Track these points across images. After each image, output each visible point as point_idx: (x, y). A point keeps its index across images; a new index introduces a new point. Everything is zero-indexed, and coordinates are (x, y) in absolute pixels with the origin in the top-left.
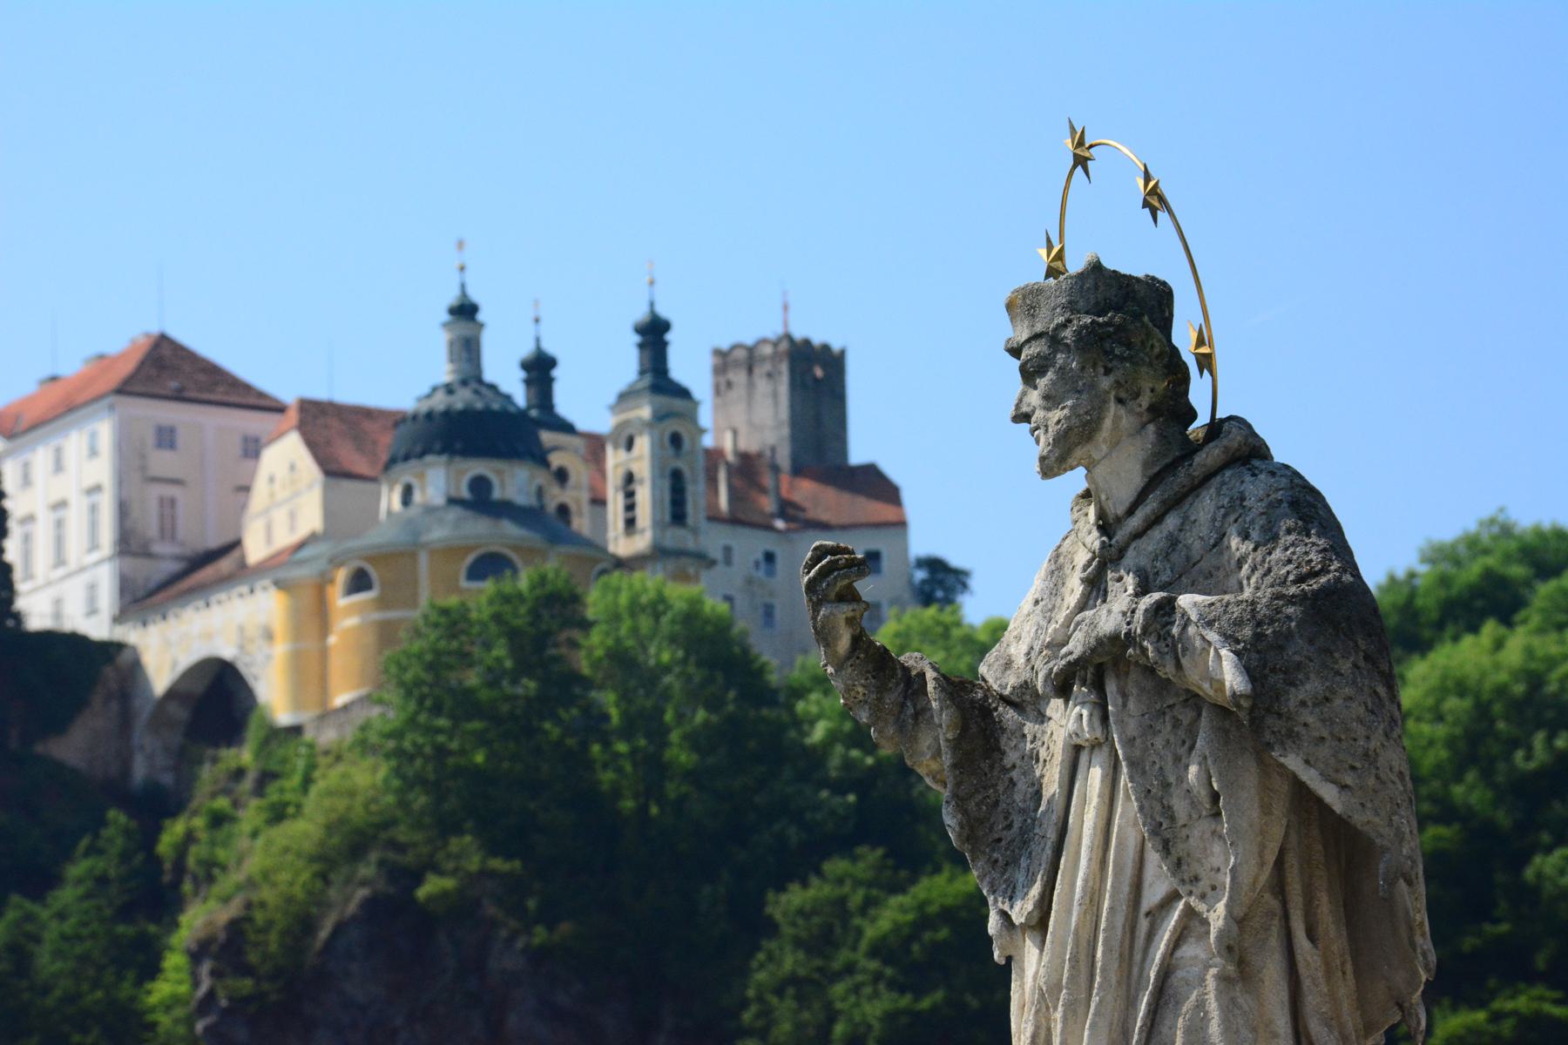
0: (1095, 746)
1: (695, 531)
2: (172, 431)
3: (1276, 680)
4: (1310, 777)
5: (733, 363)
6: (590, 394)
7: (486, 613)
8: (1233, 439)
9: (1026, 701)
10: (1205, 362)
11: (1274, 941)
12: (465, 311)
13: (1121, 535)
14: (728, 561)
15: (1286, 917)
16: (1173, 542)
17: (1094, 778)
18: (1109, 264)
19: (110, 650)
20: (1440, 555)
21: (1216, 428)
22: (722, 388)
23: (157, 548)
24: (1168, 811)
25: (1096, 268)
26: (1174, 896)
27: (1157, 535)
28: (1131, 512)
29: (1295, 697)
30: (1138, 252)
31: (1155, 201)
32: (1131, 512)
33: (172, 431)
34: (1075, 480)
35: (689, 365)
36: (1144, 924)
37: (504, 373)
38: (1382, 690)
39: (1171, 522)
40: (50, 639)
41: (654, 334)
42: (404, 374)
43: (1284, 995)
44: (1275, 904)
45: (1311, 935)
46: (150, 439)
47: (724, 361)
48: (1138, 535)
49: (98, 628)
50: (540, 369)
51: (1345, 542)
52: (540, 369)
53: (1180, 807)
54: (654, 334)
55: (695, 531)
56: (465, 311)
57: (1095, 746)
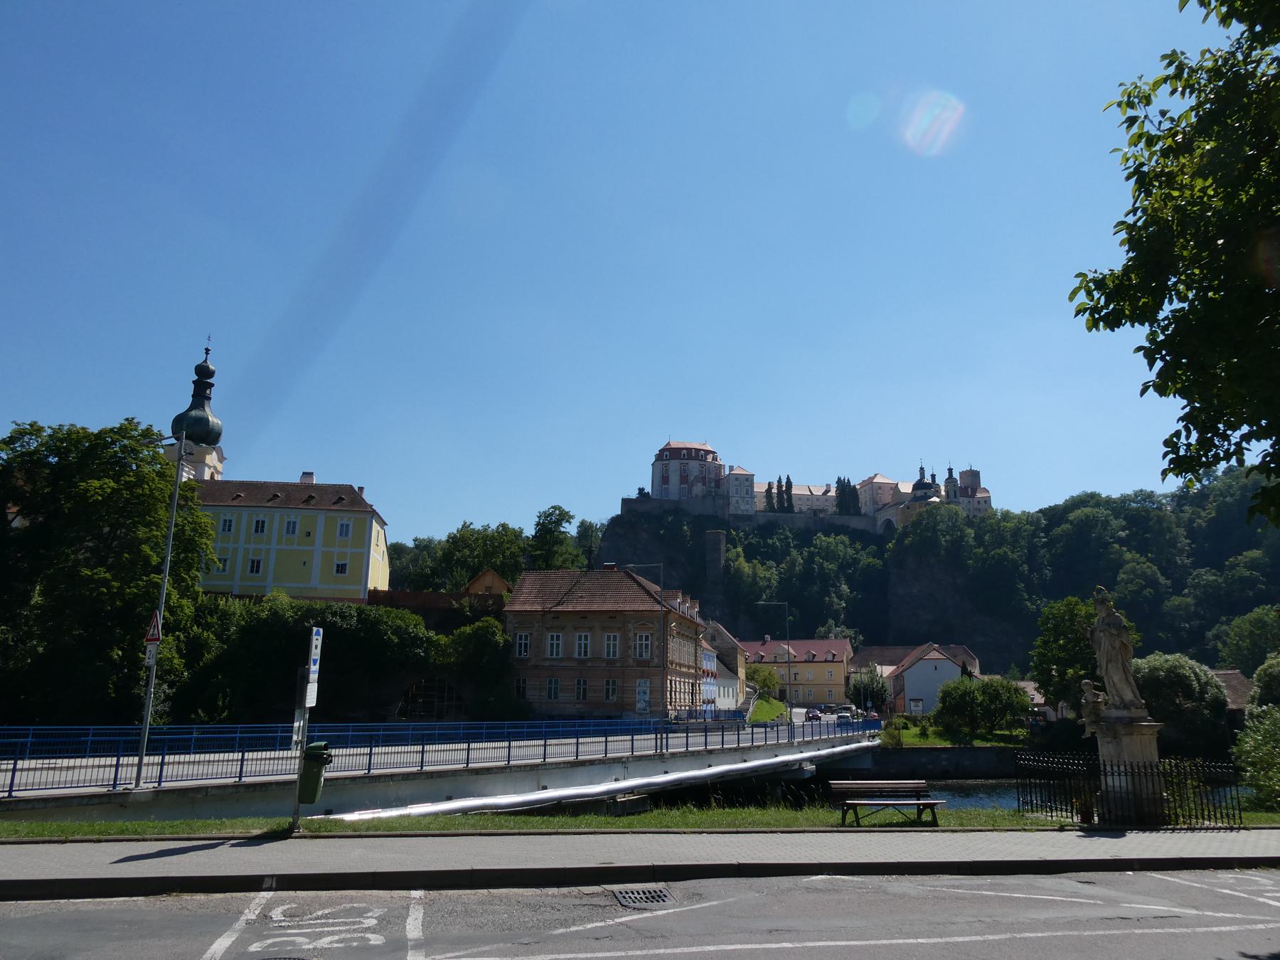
12: (922, 469)
35: (956, 475)
41: (950, 470)
50: (933, 476)
52: (933, 476)
54: (950, 470)
56: (922, 469)
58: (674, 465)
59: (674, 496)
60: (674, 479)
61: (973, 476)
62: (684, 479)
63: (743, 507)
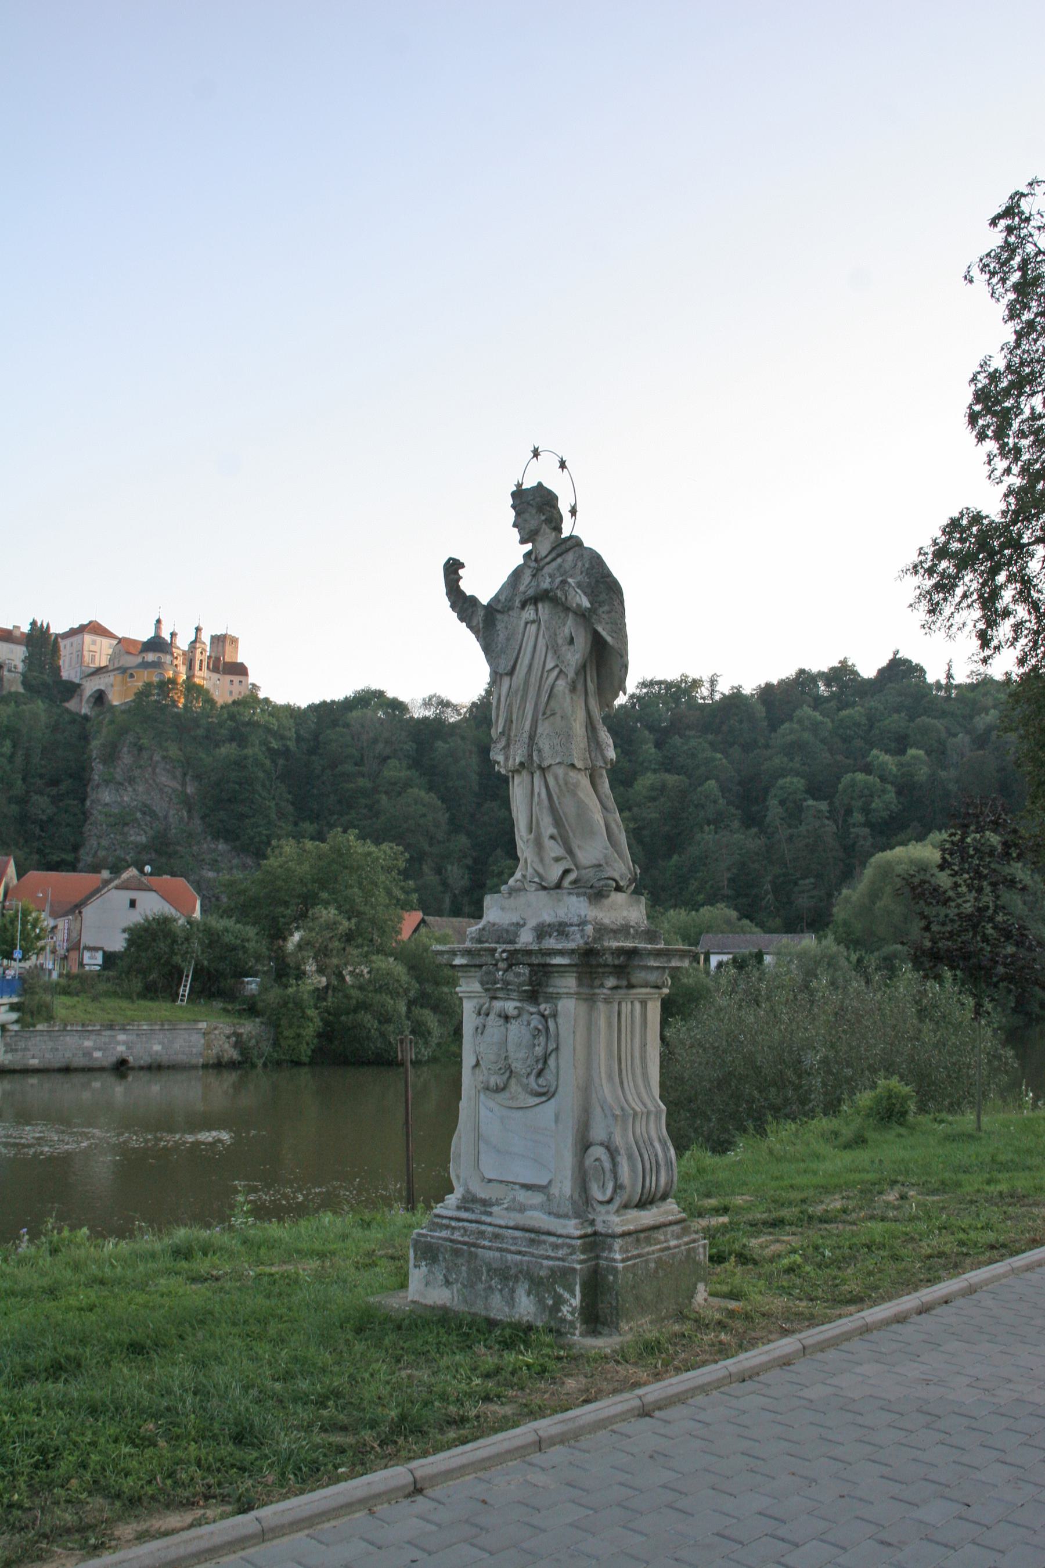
0: (533, 622)
3: (596, 605)
4: (604, 633)
6: (183, 643)
8: (573, 541)
10: (573, 512)
12: (159, 621)
13: (542, 564)
16: (560, 566)
17: (533, 628)
19: (79, 686)
20: (357, 692)
21: (571, 537)
22: (212, 643)
24: (556, 642)
26: (557, 666)
27: (554, 564)
28: (546, 557)
29: (601, 610)
31: (563, 465)
32: (546, 557)
34: (529, 547)
35: (206, 638)
36: (545, 674)
37: (166, 635)
39: (559, 560)
40: (67, 682)
41: (198, 629)
42: (145, 634)
47: (213, 637)
48: (548, 563)
49: (77, 681)
50: (173, 635)
51: (609, 575)
52: (173, 635)
53: (560, 641)
54: (198, 629)
56: (159, 621)
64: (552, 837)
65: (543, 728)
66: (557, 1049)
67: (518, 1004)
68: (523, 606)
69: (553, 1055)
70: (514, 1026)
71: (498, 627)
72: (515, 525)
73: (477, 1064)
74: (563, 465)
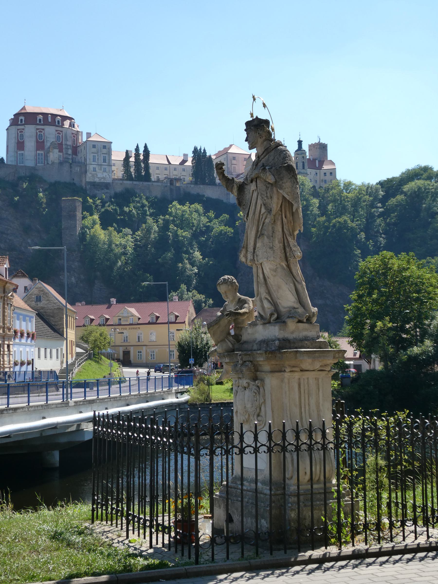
0: (256, 190)
1: (306, 170)
2: (105, 146)
5: (311, 147)
7: (285, 180)
9: (402, 192)
11: (280, 218)
14: (311, 174)
15: (282, 214)
18: (259, 117)
23: (233, 174)
25: (257, 117)
28: (262, 155)
30: (263, 115)
31: (264, 106)
32: (262, 155)
33: (105, 146)
35: (305, 147)
38: (295, 181)
41: (300, 142)
43: (281, 226)
44: (281, 213)
45: (285, 217)
46: (232, 158)
48: (262, 158)
54: (300, 142)
55: (306, 170)
57: (256, 190)
58: (30, 131)
59: (30, 163)
60: (30, 145)
61: (321, 148)
62: (40, 144)
63: (100, 175)
64: (266, 299)
65: (258, 245)
66: (264, 402)
67: (248, 381)
68: (252, 182)
69: (263, 405)
70: (247, 391)
71: (246, 192)
72: (246, 141)
73: (237, 412)
74: (264, 106)
